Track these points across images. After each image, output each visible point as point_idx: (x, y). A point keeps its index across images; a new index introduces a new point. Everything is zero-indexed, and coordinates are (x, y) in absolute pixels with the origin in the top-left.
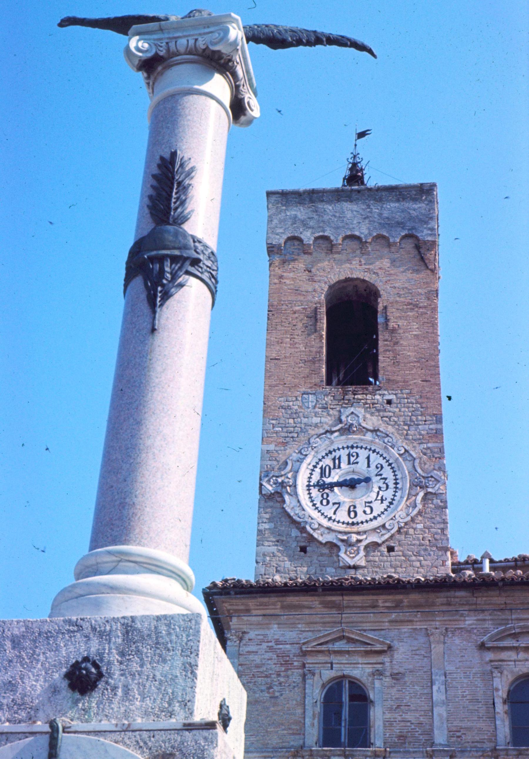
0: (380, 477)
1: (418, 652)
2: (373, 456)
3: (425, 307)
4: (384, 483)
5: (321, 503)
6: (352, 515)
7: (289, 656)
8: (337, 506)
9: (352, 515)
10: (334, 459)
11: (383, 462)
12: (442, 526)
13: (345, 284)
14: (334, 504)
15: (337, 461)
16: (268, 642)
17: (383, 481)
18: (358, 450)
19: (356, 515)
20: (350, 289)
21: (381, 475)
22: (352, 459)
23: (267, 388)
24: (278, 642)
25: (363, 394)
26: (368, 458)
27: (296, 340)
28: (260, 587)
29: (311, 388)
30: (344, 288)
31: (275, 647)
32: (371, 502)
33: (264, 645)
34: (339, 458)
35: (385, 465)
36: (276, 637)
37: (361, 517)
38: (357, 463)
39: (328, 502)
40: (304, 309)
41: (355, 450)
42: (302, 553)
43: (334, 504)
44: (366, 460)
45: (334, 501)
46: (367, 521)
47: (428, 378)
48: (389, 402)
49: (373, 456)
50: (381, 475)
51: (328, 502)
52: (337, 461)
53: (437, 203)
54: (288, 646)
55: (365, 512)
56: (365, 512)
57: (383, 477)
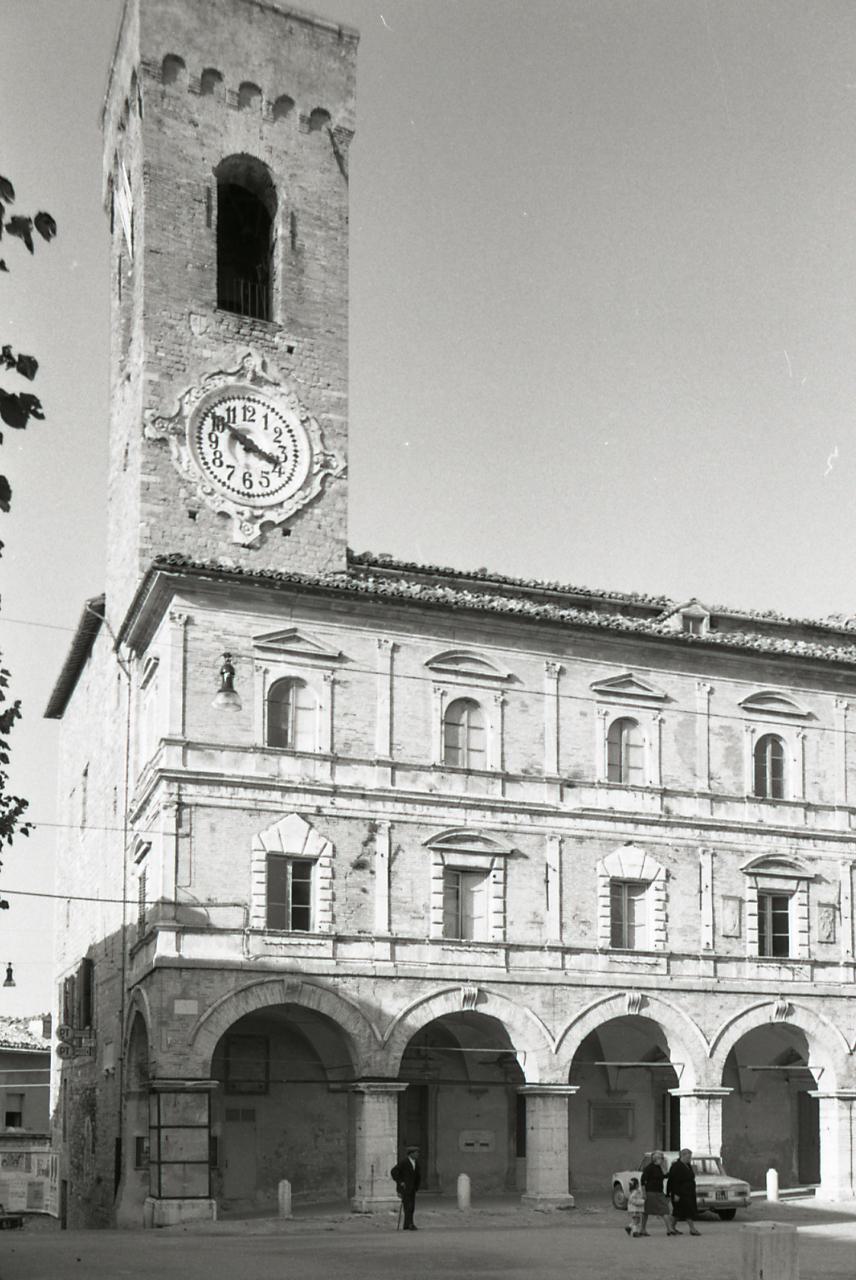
0: (278, 444)
1: (365, 663)
2: (271, 416)
3: (336, 229)
4: (283, 452)
5: (214, 461)
6: (248, 483)
7: (237, 649)
8: (231, 470)
9: (248, 483)
10: (228, 410)
11: (283, 426)
12: (342, 516)
13: (238, 161)
14: (228, 467)
15: (232, 413)
16: (215, 630)
17: (281, 450)
18: (255, 405)
19: (251, 487)
20: (241, 169)
21: (279, 442)
22: (248, 414)
23: (148, 292)
24: (226, 632)
25: (261, 331)
26: (266, 417)
27: (182, 232)
28: (212, 570)
29: (202, 306)
30: (236, 166)
31: (223, 637)
32: (267, 473)
33: (212, 634)
34: (234, 410)
35: (285, 430)
36: (224, 626)
37: (256, 489)
38: (253, 421)
39: (221, 464)
40: (189, 184)
41: (252, 404)
42: (191, 520)
43: (228, 467)
44: (264, 420)
45: (229, 464)
46: (263, 495)
47: (333, 330)
48: (290, 350)
49: (271, 416)
50: (279, 442)
51: (221, 464)
52: (232, 413)
53: (635, 814)
54: (236, 638)
55: (261, 483)
56: (261, 483)
57: (281, 444)
